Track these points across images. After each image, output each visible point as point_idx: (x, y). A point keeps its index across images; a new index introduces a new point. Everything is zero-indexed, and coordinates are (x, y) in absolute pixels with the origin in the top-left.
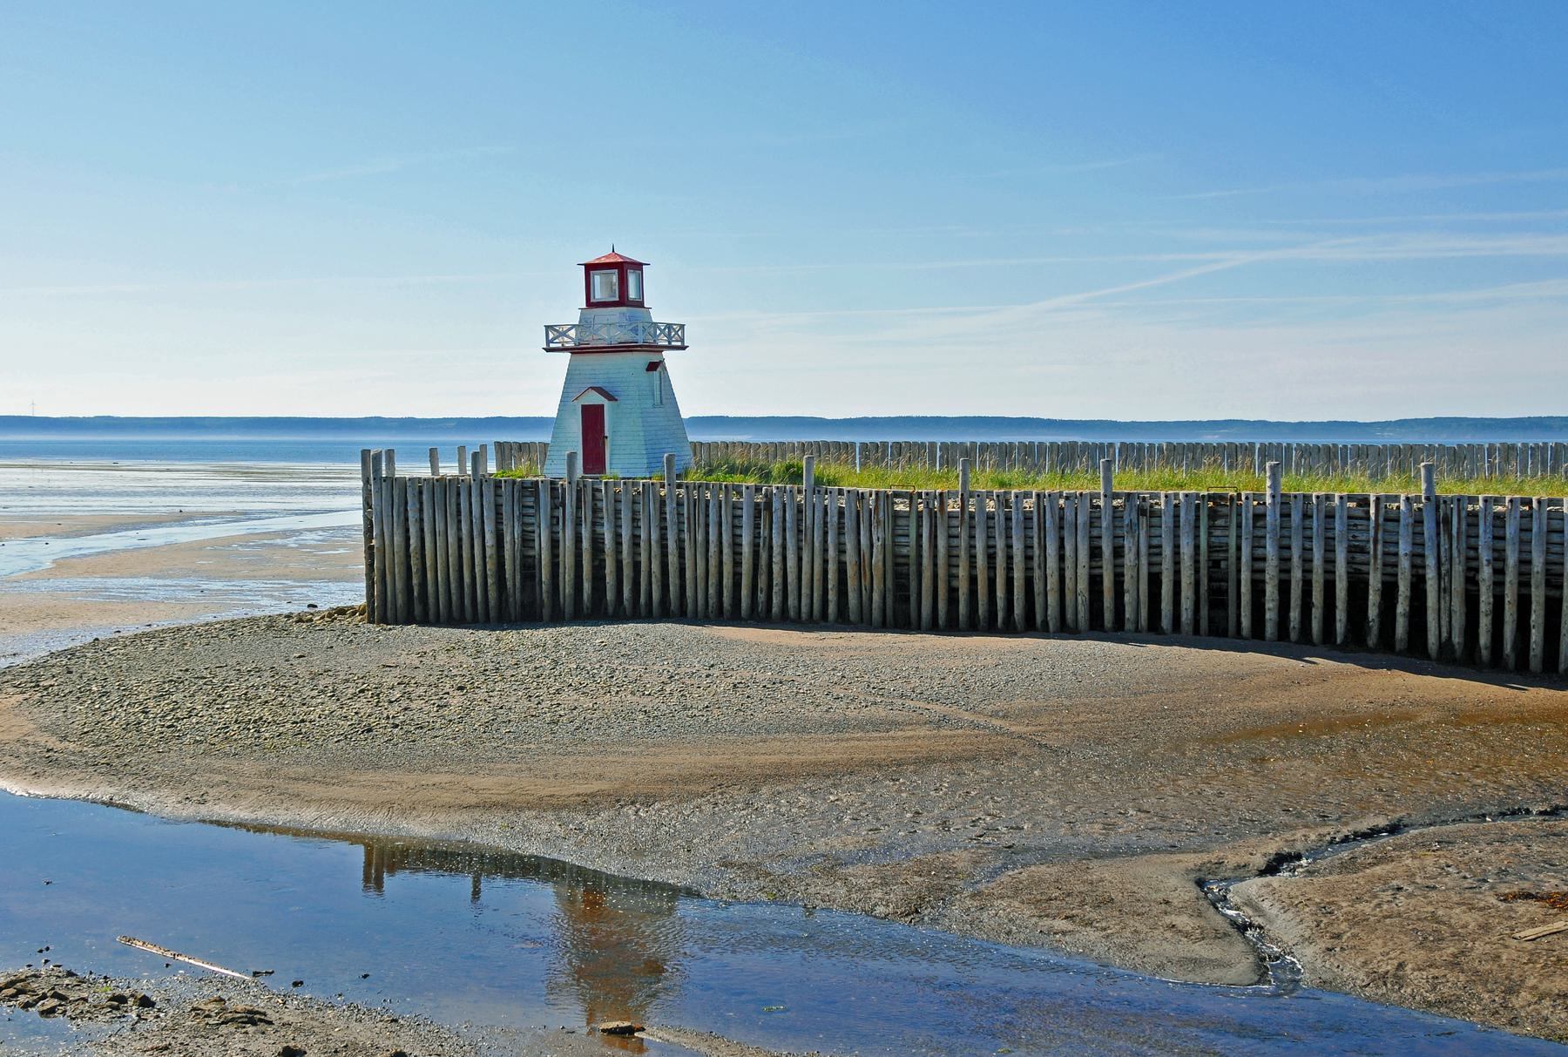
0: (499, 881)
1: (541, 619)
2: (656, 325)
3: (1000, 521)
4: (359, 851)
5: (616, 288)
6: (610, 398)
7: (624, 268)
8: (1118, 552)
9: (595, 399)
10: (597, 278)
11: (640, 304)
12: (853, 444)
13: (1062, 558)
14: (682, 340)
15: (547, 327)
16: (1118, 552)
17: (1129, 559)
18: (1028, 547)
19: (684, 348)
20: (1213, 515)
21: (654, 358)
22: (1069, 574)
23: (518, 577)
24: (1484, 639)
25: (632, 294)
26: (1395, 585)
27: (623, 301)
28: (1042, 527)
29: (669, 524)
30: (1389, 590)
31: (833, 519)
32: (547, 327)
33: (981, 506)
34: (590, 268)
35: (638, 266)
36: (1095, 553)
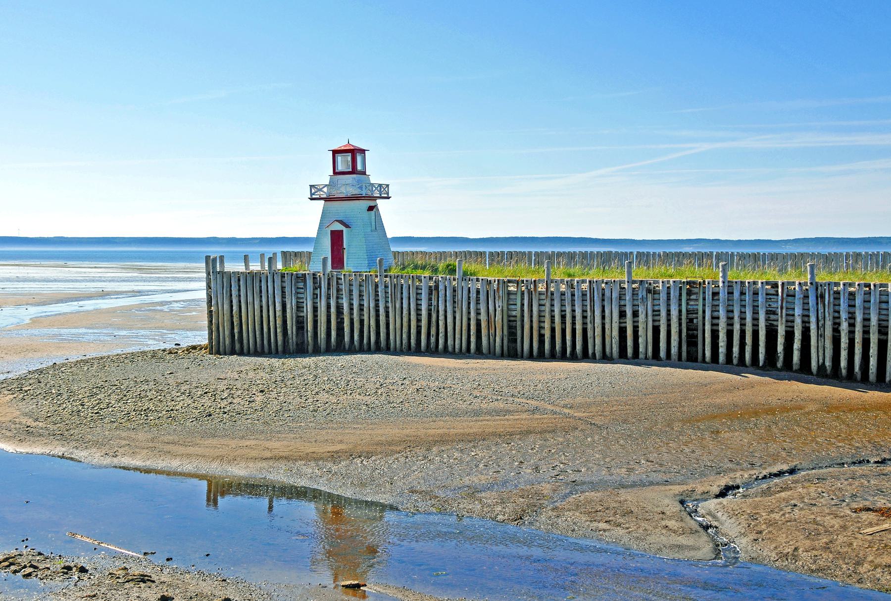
1: (308, 352)
10: (339, 158)
14: (388, 194)
19: (388, 198)
23: (294, 328)
24: (347, 338)
29: (380, 298)
31: (473, 295)
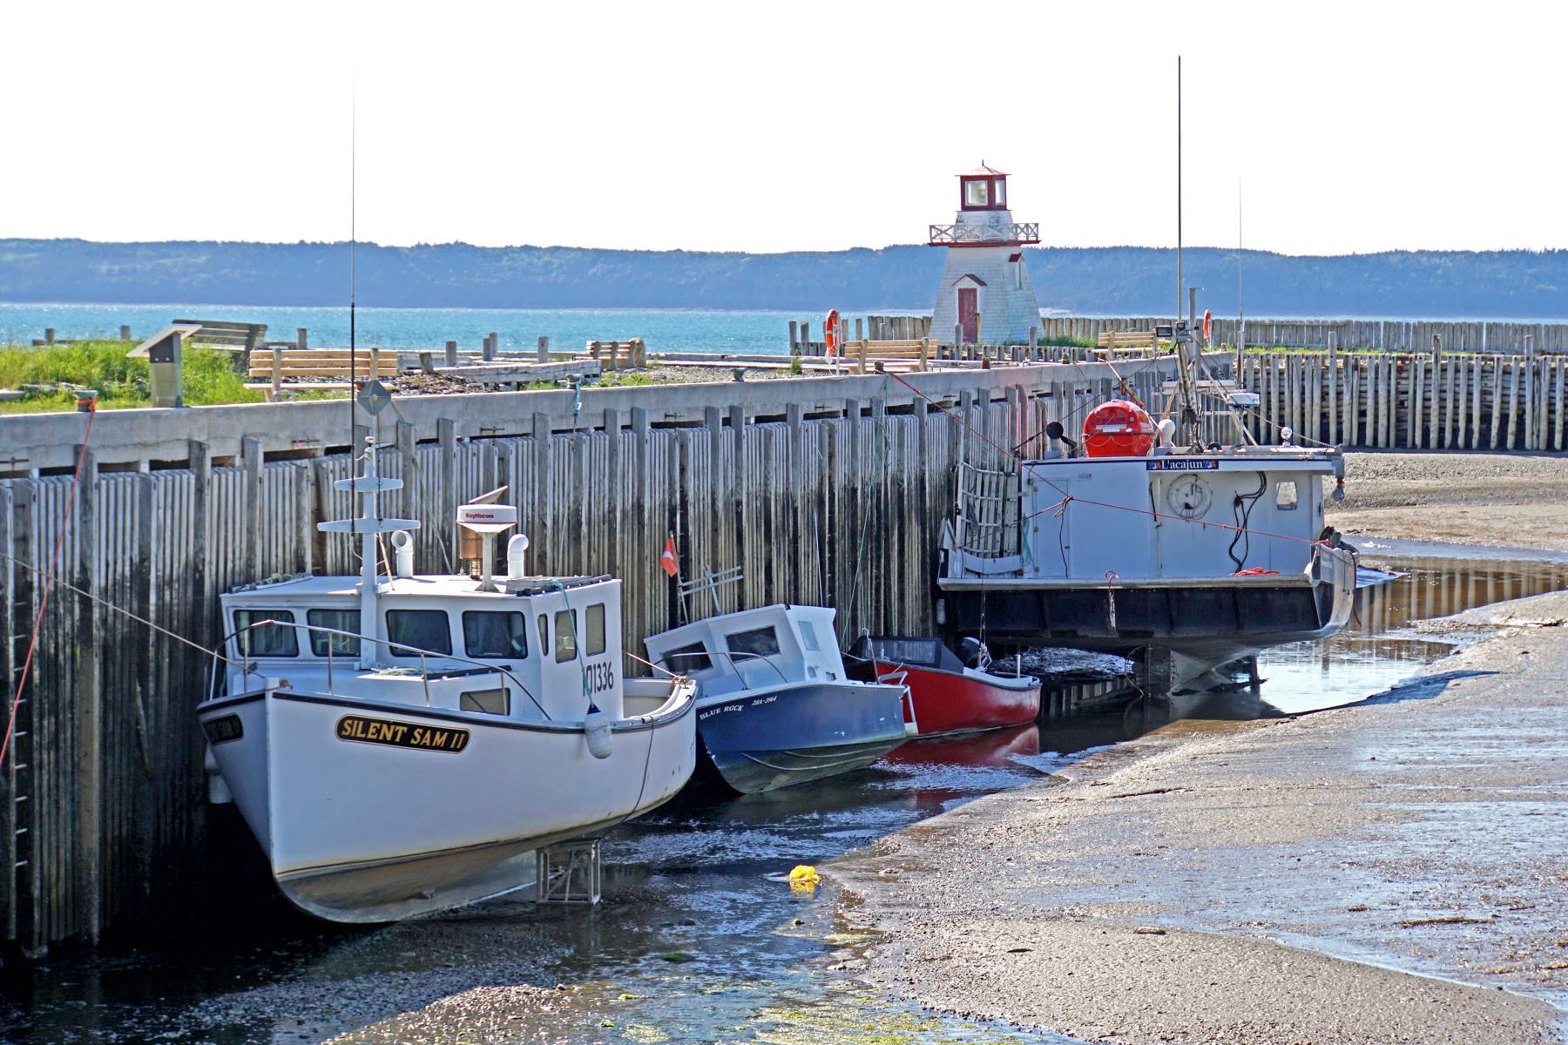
0: (1170, 247)
2: (1017, 226)
3: (1263, 376)
4: (529, 856)
5: (985, 193)
6: (982, 284)
7: (994, 180)
8: (1339, 394)
9: (969, 284)
11: (1003, 207)
12: (1377, 324)
13: (1303, 401)
15: (932, 227)
16: (1339, 394)
17: (1346, 399)
18: (1281, 393)
20: (1400, 370)
21: (1015, 250)
22: (1307, 409)
25: (998, 200)
26: (1507, 416)
27: (991, 206)
28: (1290, 378)
30: (1504, 418)
32: (932, 227)
33: (1250, 364)
34: (964, 179)
35: (1003, 177)
36: (1324, 396)
